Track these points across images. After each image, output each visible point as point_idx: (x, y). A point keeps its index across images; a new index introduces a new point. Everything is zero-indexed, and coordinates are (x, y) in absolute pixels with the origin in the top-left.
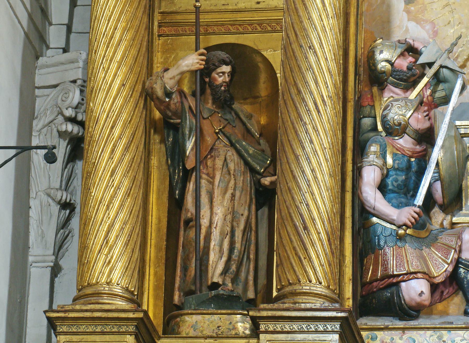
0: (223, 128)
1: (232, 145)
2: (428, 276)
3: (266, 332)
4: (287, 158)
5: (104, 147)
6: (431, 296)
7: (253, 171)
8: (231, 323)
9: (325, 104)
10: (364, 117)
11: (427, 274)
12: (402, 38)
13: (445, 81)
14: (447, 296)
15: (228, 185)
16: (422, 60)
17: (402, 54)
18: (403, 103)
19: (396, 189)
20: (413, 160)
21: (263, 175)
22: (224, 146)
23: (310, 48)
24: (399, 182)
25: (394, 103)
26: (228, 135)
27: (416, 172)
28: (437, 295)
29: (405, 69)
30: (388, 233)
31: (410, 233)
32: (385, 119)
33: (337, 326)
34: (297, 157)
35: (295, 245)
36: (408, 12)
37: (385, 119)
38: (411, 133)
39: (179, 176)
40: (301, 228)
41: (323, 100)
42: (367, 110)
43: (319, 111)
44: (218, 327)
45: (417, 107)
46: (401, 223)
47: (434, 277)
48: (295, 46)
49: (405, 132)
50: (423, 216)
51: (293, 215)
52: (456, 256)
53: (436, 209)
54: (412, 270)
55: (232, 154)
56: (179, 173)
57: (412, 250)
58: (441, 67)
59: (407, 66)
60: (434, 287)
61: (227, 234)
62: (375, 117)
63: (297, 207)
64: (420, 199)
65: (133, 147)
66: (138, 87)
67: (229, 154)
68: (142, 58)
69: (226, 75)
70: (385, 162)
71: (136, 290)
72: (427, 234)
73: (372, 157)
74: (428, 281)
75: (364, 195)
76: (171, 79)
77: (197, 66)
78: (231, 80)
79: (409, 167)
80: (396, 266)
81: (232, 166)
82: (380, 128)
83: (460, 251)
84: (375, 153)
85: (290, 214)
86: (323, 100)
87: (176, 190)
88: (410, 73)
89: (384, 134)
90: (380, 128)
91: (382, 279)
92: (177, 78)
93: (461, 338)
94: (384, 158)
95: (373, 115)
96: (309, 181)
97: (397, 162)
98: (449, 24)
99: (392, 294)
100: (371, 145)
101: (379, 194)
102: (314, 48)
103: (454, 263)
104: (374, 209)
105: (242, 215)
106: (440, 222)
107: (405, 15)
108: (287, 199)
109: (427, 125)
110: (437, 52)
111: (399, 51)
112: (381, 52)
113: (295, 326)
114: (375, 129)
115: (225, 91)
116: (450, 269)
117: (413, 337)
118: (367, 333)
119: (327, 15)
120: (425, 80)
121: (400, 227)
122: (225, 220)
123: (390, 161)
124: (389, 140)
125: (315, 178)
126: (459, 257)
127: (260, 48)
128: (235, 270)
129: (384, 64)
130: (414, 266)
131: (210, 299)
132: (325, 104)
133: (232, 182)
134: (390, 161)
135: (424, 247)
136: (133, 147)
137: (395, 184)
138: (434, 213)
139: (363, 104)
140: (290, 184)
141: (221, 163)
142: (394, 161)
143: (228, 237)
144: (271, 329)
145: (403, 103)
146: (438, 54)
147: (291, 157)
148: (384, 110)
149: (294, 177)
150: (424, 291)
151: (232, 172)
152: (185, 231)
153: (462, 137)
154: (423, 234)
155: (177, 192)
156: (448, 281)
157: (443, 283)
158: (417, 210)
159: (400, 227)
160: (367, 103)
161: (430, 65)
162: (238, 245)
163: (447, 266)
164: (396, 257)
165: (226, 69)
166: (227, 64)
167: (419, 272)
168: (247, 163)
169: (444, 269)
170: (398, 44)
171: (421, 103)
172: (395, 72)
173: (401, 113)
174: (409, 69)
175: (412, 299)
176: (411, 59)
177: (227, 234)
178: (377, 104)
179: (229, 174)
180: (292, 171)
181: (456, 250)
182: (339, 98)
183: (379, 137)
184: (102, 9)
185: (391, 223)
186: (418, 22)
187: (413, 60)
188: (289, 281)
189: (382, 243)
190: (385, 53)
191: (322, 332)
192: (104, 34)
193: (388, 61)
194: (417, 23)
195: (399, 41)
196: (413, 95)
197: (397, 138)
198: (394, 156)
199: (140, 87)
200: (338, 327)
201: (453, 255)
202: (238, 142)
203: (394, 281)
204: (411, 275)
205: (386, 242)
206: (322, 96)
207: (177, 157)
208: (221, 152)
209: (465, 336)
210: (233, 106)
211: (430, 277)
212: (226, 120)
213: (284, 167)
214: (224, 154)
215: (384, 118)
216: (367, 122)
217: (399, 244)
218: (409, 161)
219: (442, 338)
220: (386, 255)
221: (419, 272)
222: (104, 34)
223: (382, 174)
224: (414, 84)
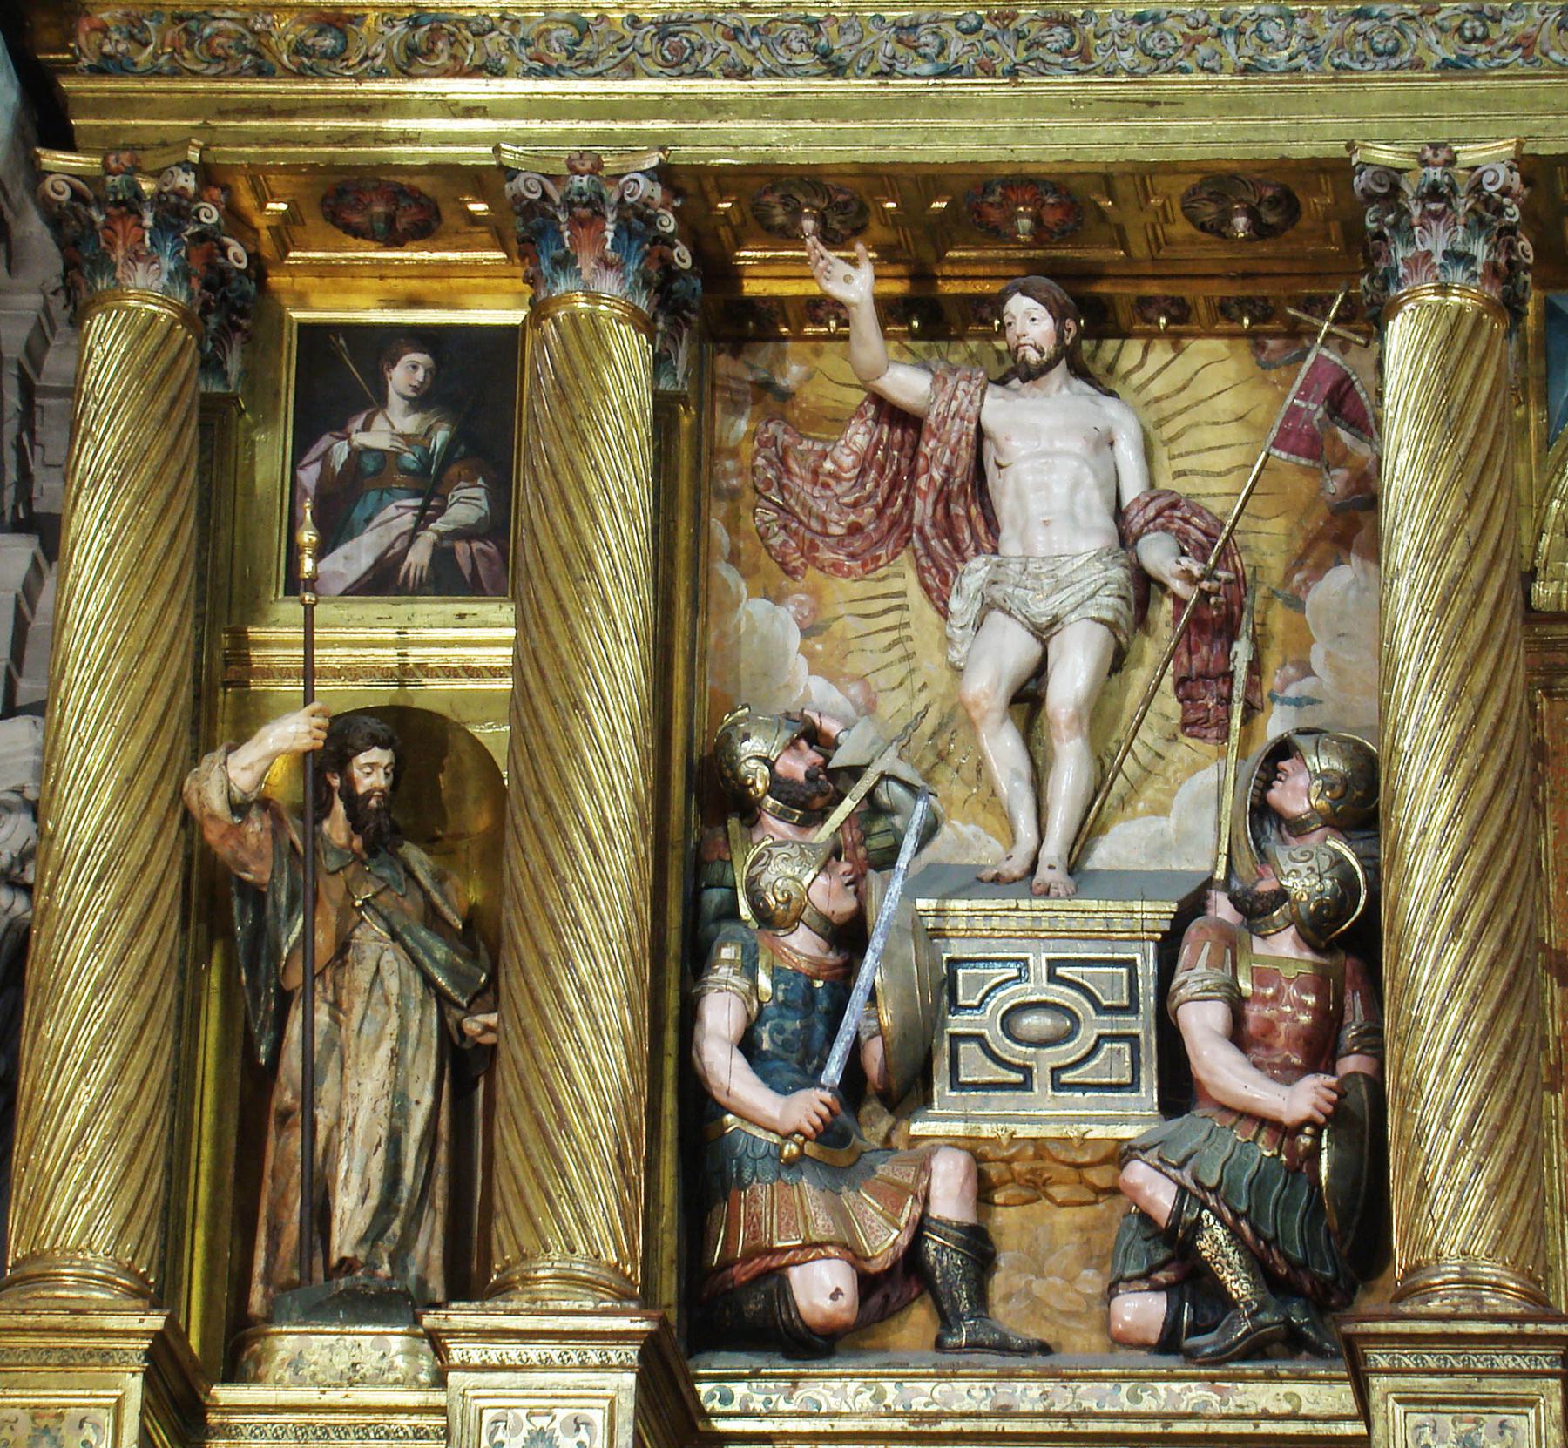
0: (374, 896)
1: (395, 936)
2: (854, 1255)
3: (465, 1367)
4: (520, 959)
5: (78, 925)
6: (860, 1305)
7: (442, 998)
8: (384, 1355)
9: (610, 837)
10: (709, 886)
11: (850, 1249)
12: (795, 710)
13: (890, 811)
14: (897, 1307)
15: (383, 1028)
16: (839, 759)
17: (793, 744)
18: (795, 852)
19: (780, 1051)
20: (819, 984)
21: (469, 1011)
22: (376, 939)
23: (575, 706)
24: (788, 1035)
25: (775, 851)
26: (385, 912)
27: (827, 1013)
28: (876, 1300)
29: (801, 777)
30: (761, 1151)
31: (811, 1154)
32: (755, 887)
33: (631, 1352)
34: (543, 959)
35: (538, 1163)
36: (810, 655)
37: (755, 887)
38: (816, 921)
39: (266, 1011)
40: (551, 1125)
41: (607, 829)
42: (715, 871)
43: (596, 854)
44: (354, 1365)
45: (828, 860)
46: (790, 1127)
47: (867, 1259)
48: (540, 701)
49: (798, 919)
50: (843, 1117)
51: (533, 1094)
52: (918, 1211)
53: (872, 1107)
54: (815, 1238)
55: (392, 959)
56: (268, 1002)
57: (816, 1193)
58: (884, 777)
59: (807, 773)
60: (868, 1284)
61: (379, 1145)
62: (734, 888)
63: (544, 1076)
64: (833, 1071)
65: (150, 931)
66: (165, 790)
67: (388, 956)
68: (175, 721)
69: (381, 771)
70: (755, 987)
71: (153, 1272)
72: (852, 1160)
73: (723, 972)
74: (853, 1265)
75: (707, 1059)
76: (244, 769)
77: (305, 743)
78: (394, 786)
79: (810, 995)
80: (779, 1227)
81: (393, 985)
82: (745, 911)
83: (926, 1201)
84: (731, 963)
85: (525, 1090)
86: (607, 829)
87: (260, 1043)
88: (814, 789)
89: (754, 925)
90: (745, 911)
91: (748, 1256)
92: (259, 768)
93: (925, 1400)
94: (752, 976)
95: (728, 881)
96: (572, 1014)
97: (782, 986)
98: (901, 684)
99: (769, 1295)
100: (723, 945)
101: (739, 1061)
102: (585, 708)
103: (912, 1228)
104: (728, 1093)
105: (418, 1102)
106: (882, 1135)
107: (802, 660)
108: (520, 1056)
109: (847, 905)
110: (873, 743)
111: (786, 735)
112: (747, 737)
113: (534, 1352)
114: (734, 914)
115: (378, 810)
116: (904, 1240)
117: (816, 1397)
118: (712, 1385)
119: (617, 634)
120: (848, 805)
121: (787, 1137)
122: (374, 1110)
123: (764, 982)
124: (763, 940)
125: (588, 1007)
126: (924, 1214)
127: (464, 718)
128: (398, 1232)
129: (753, 763)
130: (822, 1226)
131: (335, 1296)
132: (610, 837)
133: (394, 1023)
134: (764, 982)
135: (845, 1188)
136: (150, 931)
137: (779, 1039)
138: (869, 1114)
139: (707, 858)
140: (527, 1021)
141: (368, 978)
142: (774, 985)
143: (381, 1150)
144: (476, 1361)
145: (795, 852)
146: (876, 747)
147: (531, 960)
148: (751, 867)
149: (537, 1004)
150: (843, 1288)
151: (393, 999)
152: (278, 1138)
153: (931, 938)
154: (842, 1156)
155: (263, 1049)
156: (900, 1269)
157: (888, 1273)
158: (827, 1096)
159: (787, 1137)
160: (715, 855)
161: (855, 772)
162: (408, 1175)
163: (896, 1233)
164: (779, 1208)
165: (379, 756)
166: (383, 746)
167: (830, 1243)
168: (428, 981)
169: (891, 1240)
170: (785, 722)
171: (836, 853)
172: (778, 785)
173: (789, 872)
174: (811, 777)
175: (814, 1307)
176: (813, 756)
177: (379, 1145)
178: (737, 858)
179: (387, 1003)
180: (531, 992)
181: (916, 1197)
182: (644, 828)
183: (741, 928)
184: (79, 602)
185: (768, 1130)
186: (833, 677)
187: (820, 759)
188: (520, 1248)
189: (747, 1175)
190: (754, 739)
191: (596, 1368)
192: (83, 661)
193: (765, 760)
194: (831, 681)
195: (787, 715)
196: (822, 834)
197: (781, 933)
198: (776, 974)
199: (171, 789)
200: (634, 1357)
201: (910, 1210)
202: (408, 930)
203: (774, 1264)
204: (812, 1248)
205: (754, 1173)
206: (604, 819)
207: (263, 966)
208: (368, 954)
209: (936, 1395)
210: (400, 851)
211: (855, 1256)
212: (381, 879)
213: (513, 981)
214: (375, 956)
215: (752, 882)
216: (714, 896)
217: (784, 1175)
218: (810, 986)
219: (884, 1398)
220: (756, 1202)
221: (830, 1243)
222: (83, 661)
223: (748, 1016)
224: (821, 816)
